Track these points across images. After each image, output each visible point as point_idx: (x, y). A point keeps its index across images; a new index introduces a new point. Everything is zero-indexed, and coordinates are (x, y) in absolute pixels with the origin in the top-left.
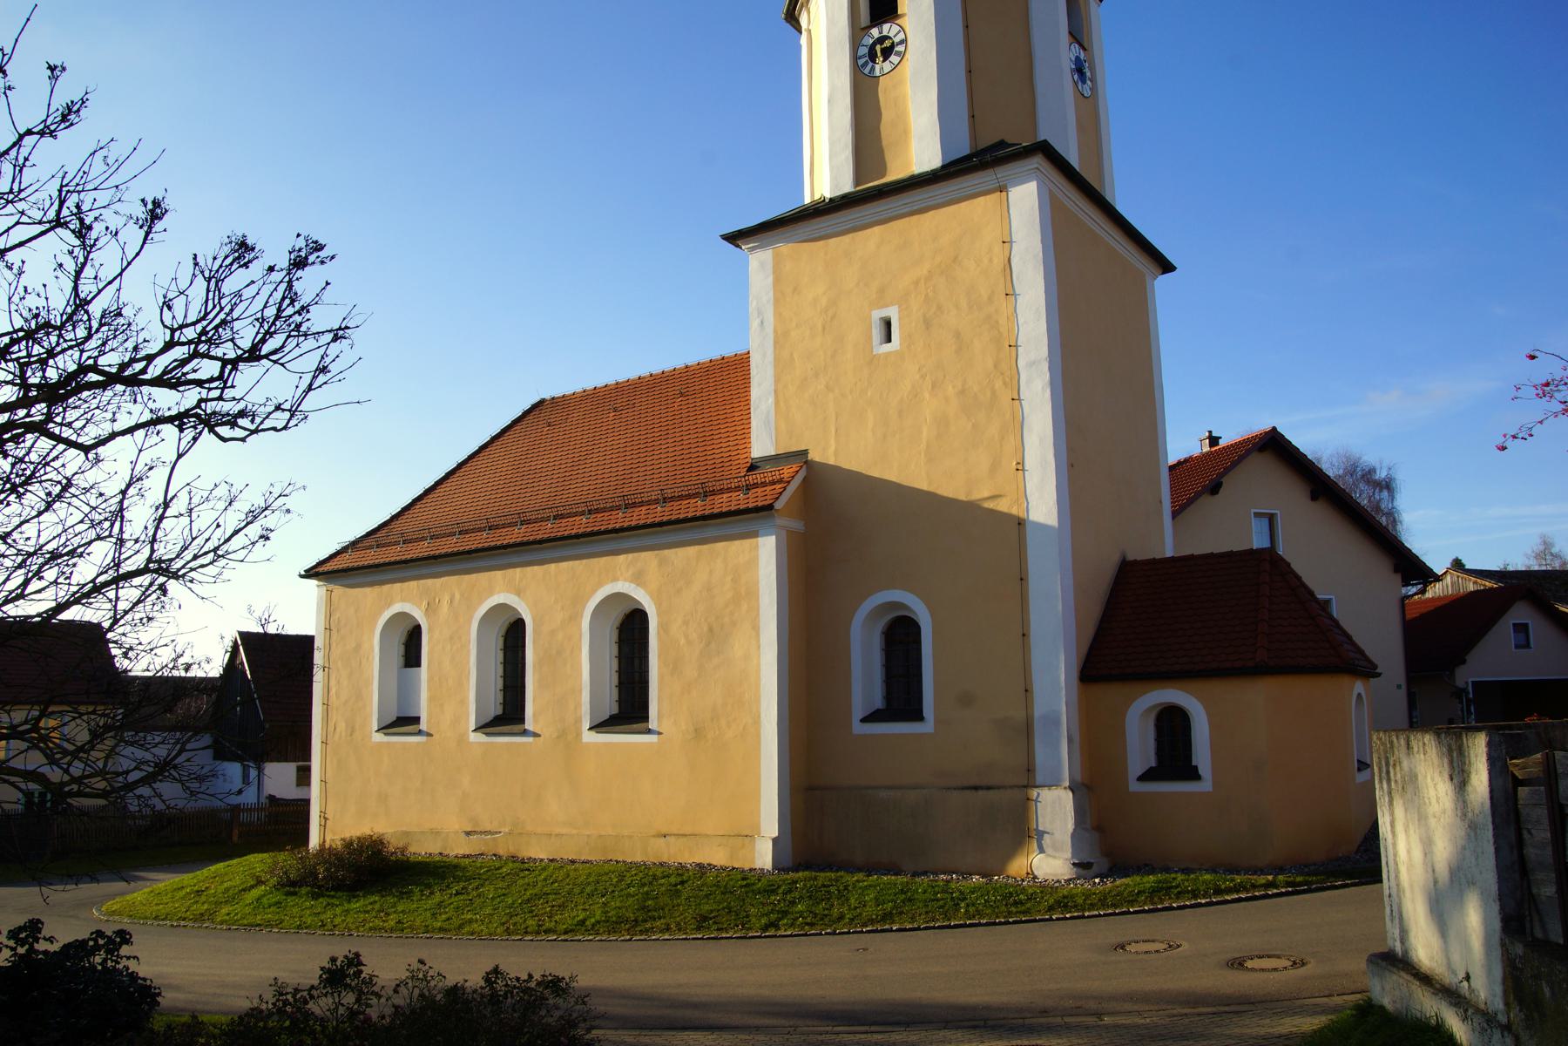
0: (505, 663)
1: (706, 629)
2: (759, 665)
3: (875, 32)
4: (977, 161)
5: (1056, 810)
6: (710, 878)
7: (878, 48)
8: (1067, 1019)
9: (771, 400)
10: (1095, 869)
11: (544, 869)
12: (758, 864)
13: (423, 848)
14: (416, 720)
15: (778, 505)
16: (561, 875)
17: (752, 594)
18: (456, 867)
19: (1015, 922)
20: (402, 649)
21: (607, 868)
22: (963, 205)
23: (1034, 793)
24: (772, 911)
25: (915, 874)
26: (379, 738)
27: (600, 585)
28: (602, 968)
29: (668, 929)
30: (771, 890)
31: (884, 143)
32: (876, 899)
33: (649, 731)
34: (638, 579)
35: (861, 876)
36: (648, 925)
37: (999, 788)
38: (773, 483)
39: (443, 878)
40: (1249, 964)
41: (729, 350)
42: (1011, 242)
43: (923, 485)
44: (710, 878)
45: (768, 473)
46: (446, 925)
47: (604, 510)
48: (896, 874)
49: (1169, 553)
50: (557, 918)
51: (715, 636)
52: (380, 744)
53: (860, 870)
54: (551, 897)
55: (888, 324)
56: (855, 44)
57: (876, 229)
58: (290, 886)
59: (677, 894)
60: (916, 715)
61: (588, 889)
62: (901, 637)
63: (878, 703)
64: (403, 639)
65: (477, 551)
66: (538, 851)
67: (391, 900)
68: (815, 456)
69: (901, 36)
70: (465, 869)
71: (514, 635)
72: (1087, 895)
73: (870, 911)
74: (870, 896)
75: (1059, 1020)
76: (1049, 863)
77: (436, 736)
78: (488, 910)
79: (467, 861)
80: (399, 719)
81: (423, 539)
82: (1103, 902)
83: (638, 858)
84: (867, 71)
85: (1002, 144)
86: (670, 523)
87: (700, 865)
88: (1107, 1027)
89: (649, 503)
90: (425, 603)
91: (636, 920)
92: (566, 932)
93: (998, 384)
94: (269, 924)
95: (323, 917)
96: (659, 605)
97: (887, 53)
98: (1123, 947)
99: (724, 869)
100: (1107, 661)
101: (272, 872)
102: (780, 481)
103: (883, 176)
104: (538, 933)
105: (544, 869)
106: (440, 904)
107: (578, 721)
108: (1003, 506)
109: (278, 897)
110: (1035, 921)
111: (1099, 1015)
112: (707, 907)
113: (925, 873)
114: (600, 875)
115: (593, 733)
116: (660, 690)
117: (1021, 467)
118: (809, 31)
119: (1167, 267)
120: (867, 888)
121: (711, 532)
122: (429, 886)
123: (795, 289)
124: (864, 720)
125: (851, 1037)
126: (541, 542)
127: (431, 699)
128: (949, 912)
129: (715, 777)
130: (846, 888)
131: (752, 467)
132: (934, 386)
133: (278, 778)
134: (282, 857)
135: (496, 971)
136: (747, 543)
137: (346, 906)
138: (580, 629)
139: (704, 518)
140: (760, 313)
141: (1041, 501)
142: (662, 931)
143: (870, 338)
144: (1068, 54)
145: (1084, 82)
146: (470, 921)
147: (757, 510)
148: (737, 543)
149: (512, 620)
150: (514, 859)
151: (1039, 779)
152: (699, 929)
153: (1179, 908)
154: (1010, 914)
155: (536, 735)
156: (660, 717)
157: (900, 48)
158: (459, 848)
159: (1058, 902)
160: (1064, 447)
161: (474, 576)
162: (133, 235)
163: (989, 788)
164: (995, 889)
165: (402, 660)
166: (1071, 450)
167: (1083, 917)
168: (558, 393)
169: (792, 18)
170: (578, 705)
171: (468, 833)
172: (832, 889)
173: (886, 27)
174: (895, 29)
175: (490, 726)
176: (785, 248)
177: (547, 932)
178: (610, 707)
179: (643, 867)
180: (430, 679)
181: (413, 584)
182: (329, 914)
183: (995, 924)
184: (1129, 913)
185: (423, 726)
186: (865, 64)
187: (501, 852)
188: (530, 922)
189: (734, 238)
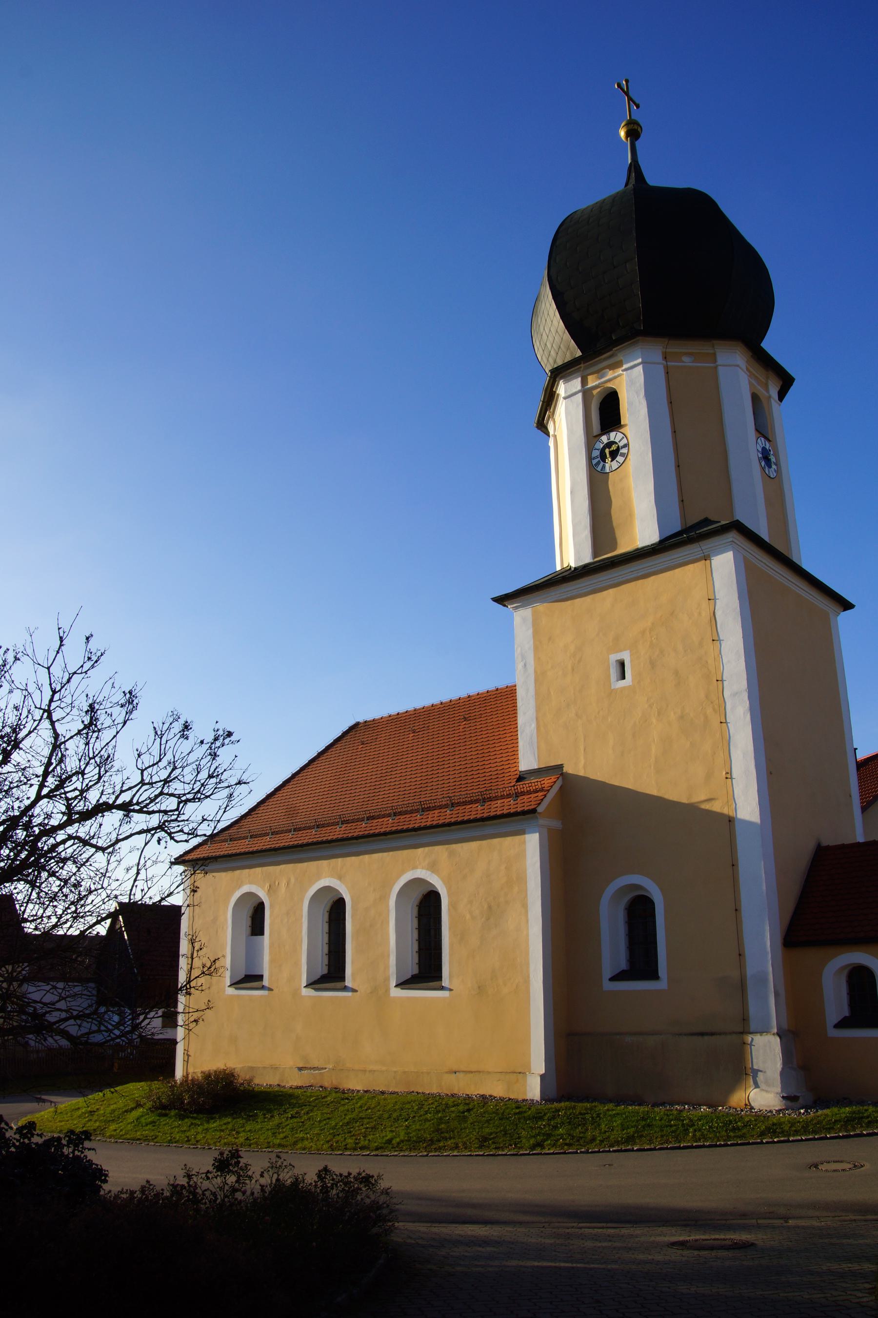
0: (330, 933)
1: (486, 907)
2: (527, 935)
3: (604, 439)
4: (686, 537)
5: (767, 1051)
6: (491, 1106)
7: (607, 451)
8: (760, 1221)
9: (534, 725)
10: (801, 1101)
11: (360, 1098)
12: (529, 1096)
13: (265, 1081)
14: (260, 978)
15: (540, 809)
16: (373, 1103)
17: (522, 879)
18: (291, 1096)
19: (732, 1145)
20: (249, 920)
21: (409, 1098)
22: (677, 571)
23: (749, 1038)
24: (539, 1134)
25: (653, 1106)
26: (231, 991)
27: (403, 872)
28: (406, 1178)
29: (457, 1147)
30: (538, 1117)
31: (614, 524)
32: (622, 1124)
33: (442, 988)
34: (433, 867)
35: (611, 1106)
36: (441, 1144)
37: (720, 1034)
38: (536, 791)
39: (281, 1105)
40: (847, 1166)
41: (501, 684)
42: (715, 599)
43: (654, 792)
44: (491, 1106)
45: (533, 782)
46: (283, 1142)
47: (406, 813)
48: (639, 1105)
49: (860, 839)
50: (370, 1137)
51: (493, 913)
52: (232, 996)
53: (611, 1101)
54: (366, 1121)
55: (622, 664)
56: (590, 448)
57: (611, 591)
58: (162, 1108)
59: (465, 1119)
60: (652, 974)
61: (395, 1115)
62: (640, 911)
63: (623, 965)
64: (250, 913)
65: (308, 845)
66: (355, 1084)
67: (241, 1121)
68: (568, 769)
69: (624, 441)
70: (297, 1097)
71: (336, 911)
72: (792, 1123)
73: (617, 1134)
74: (617, 1123)
75: (754, 1221)
76: (763, 1096)
77: (276, 991)
78: (316, 1131)
79: (300, 1091)
80: (246, 976)
81: (267, 834)
82: (805, 1129)
83: (435, 1091)
84: (599, 469)
85: (706, 522)
86: (456, 823)
87: (483, 1097)
88: (789, 1227)
89: (440, 807)
90: (267, 885)
91: (431, 1140)
92: (377, 1149)
93: (709, 711)
94: (146, 1139)
95: (188, 1134)
96: (449, 890)
97: (614, 455)
98: (816, 1166)
99: (502, 1099)
100: (807, 928)
101: (148, 1097)
102: (542, 790)
103: (615, 549)
104: (355, 1149)
105: (360, 1098)
106: (279, 1126)
107: (387, 980)
108: (716, 807)
109: (152, 1117)
110: (749, 1144)
111: (786, 1219)
112: (487, 1130)
113: (663, 1104)
114: (404, 1103)
115: (398, 990)
116: (451, 955)
117: (729, 776)
118: (555, 436)
119: (847, 605)
120: (615, 1117)
121: (488, 831)
122: (270, 1111)
123: (550, 639)
124: (611, 979)
125: (590, 1231)
126: (357, 838)
127: (272, 961)
128: (680, 1136)
129: (494, 1027)
130: (598, 1115)
131: (521, 778)
132: (659, 713)
133: (153, 1023)
134: (155, 1085)
135: (326, 1169)
136: (517, 839)
137: (206, 1126)
138: (388, 906)
139: (483, 819)
140: (523, 657)
141: (746, 804)
142: (452, 1149)
143: (609, 676)
144: (754, 445)
145: (770, 467)
146: (302, 1139)
147: (524, 813)
148: (509, 839)
149: (336, 899)
150: (336, 1089)
151: (753, 1027)
152: (481, 1147)
153: (869, 1135)
154: (729, 1138)
155: (354, 991)
156: (451, 977)
157: (624, 451)
158: (294, 1080)
159: (768, 1129)
160: (764, 759)
161: (306, 864)
162: (119, 714)
163: (712, 1034)
164: (718, 1118)
165: (249, 930)
166: (768, 760)
167: (788, 1141)
168: (369, 717)
169: (542, 426)
170: (387, 967)
171: (300, 1069)
172: (587, 1116)
173: (613, 434)
174: (620, 436)
175: (319, 982)
176: (541, 607)
177: (362, 1148)
178: (412, 968)
179: (437, 1098)
180: (271, 946)
181: (258, 870)
182: (193, 1132)
183: (716, 1146)
184: (826, 1138)
185: (266, 982)
186: (598, 463)
187: (326, 1084)
188: (350, 1141)
189: (502, 600)
